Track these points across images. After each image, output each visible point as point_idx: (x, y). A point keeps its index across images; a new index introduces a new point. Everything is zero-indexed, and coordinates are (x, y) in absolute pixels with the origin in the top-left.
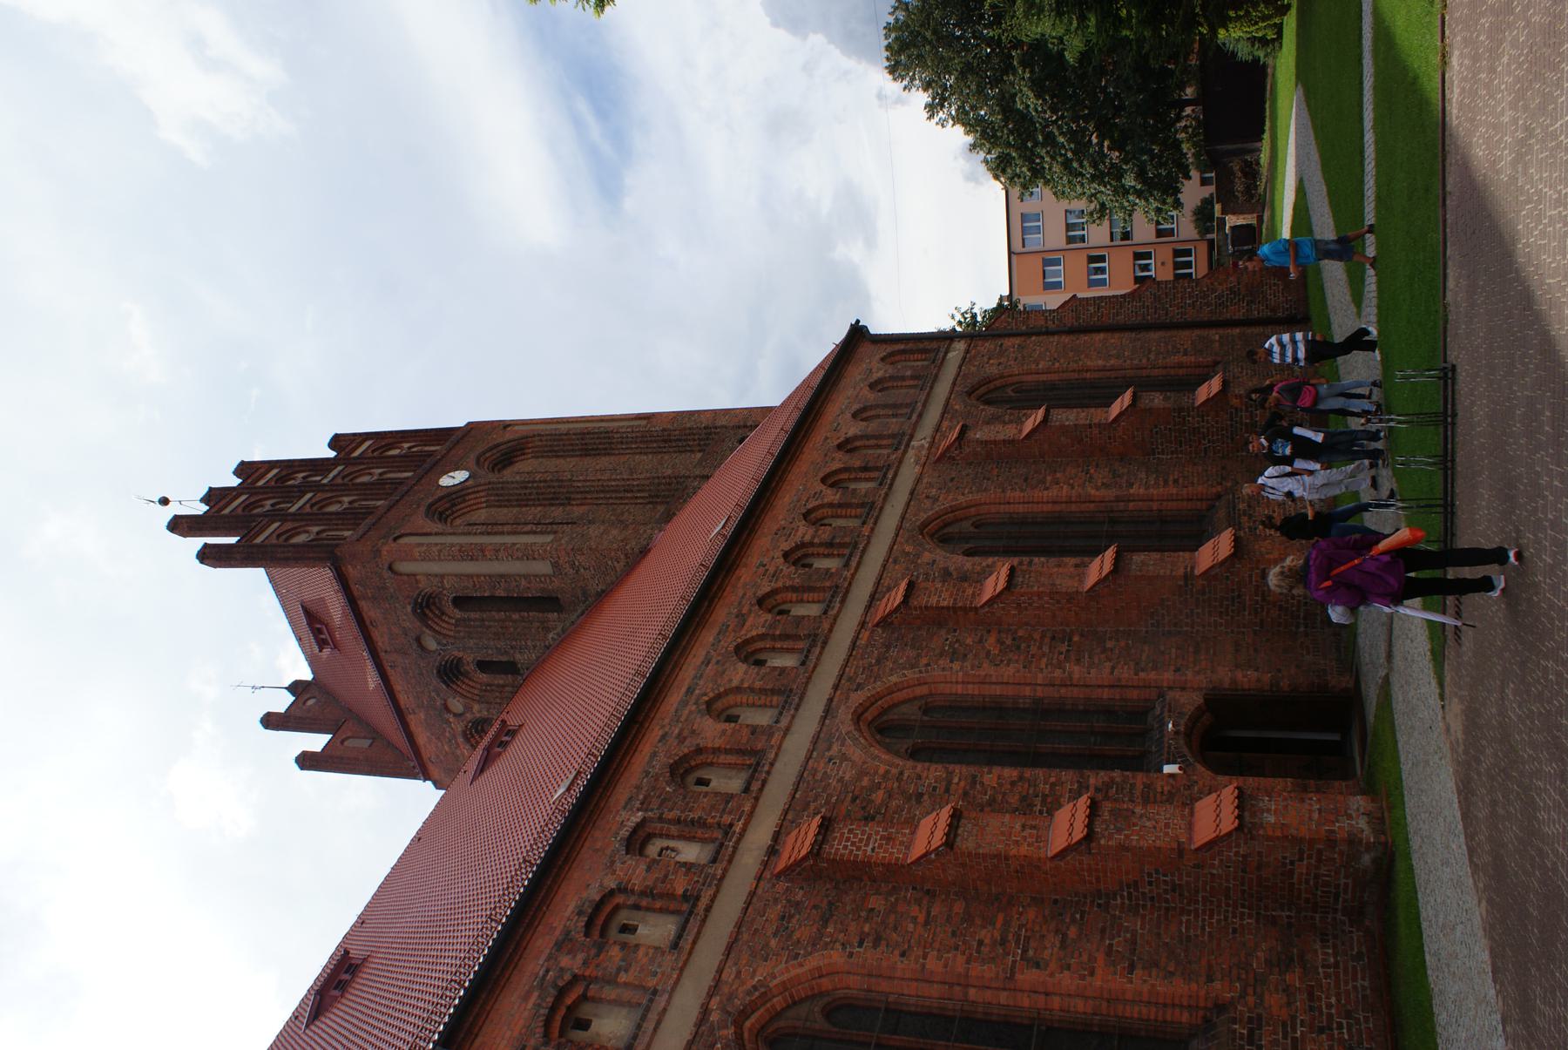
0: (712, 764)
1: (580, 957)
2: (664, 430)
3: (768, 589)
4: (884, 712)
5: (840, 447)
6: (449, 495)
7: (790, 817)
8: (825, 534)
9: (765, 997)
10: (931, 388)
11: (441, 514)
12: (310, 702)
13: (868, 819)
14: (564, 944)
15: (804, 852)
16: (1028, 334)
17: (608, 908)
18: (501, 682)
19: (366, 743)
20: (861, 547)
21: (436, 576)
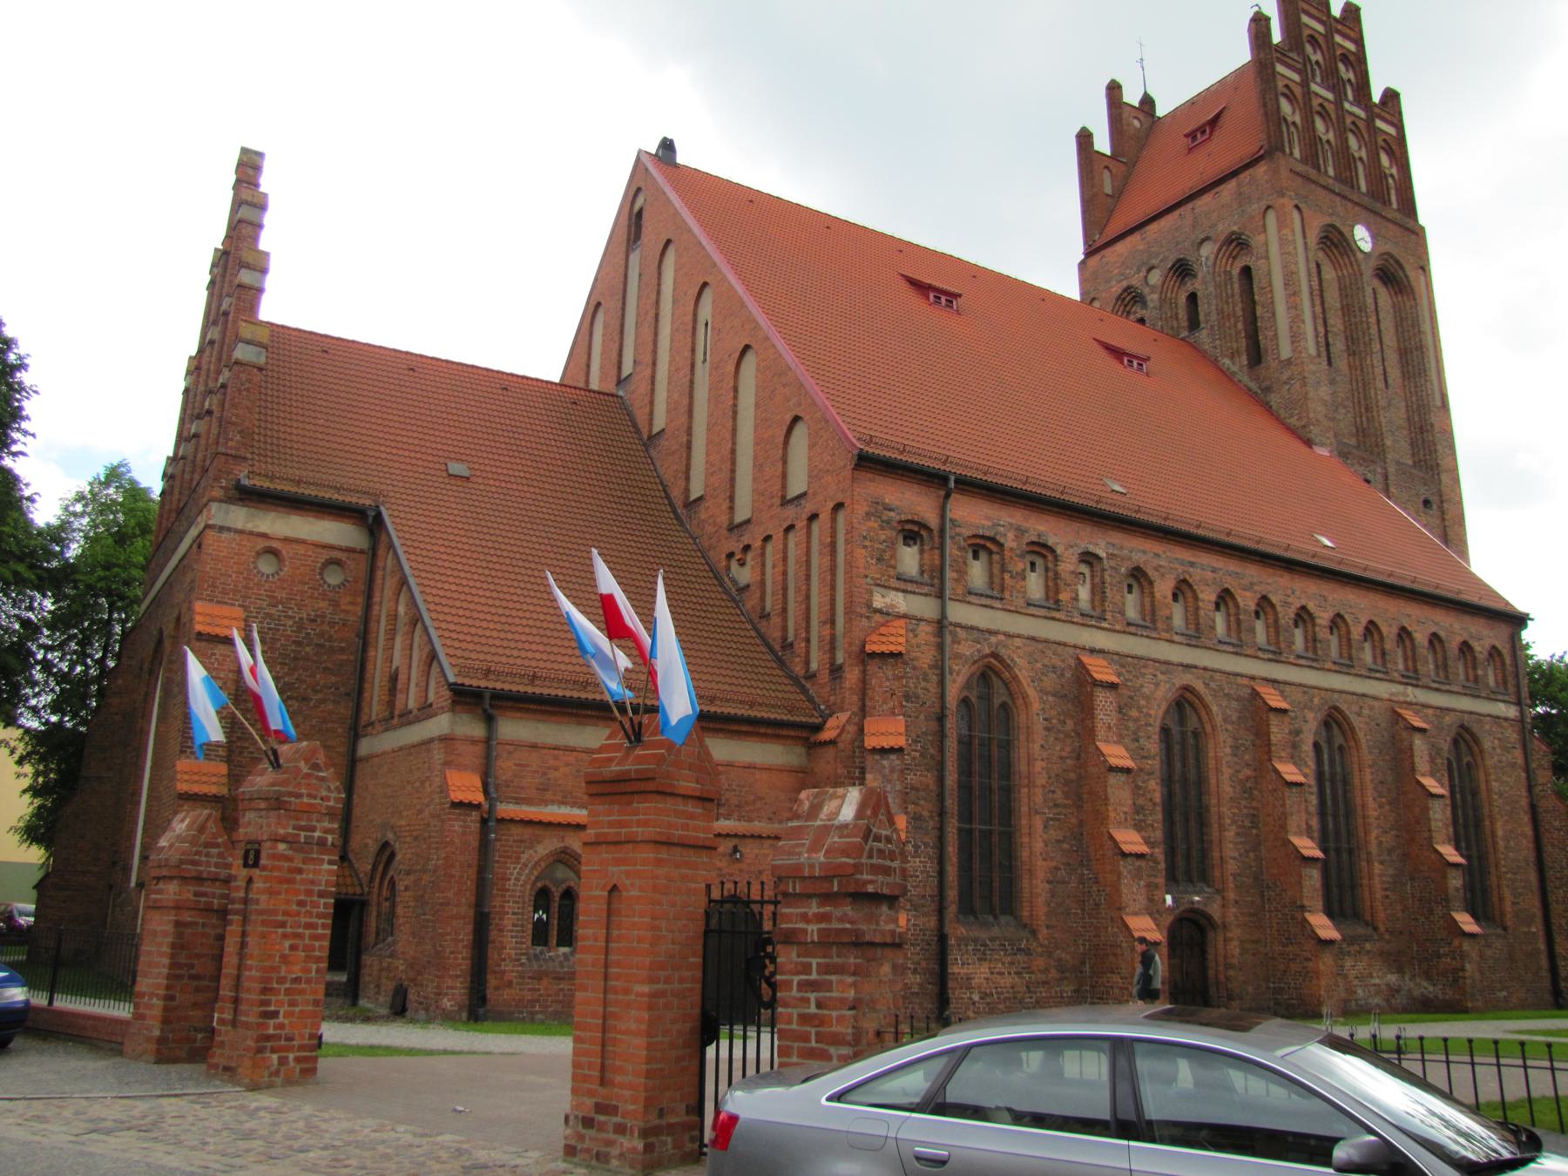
0: (1143, 592)
1: (1014, 545)
2: (1432, 425)
3: (1274, 601)
4: (1192, 705)
5: (1403, 629)
6: (1346, 240)
7: (1115, 657)
8: (1323, 634)
9: (1008, 667)
10: (1465, 694)
11: (1326, 237)
12: (1136, 123)
13: (1120, 710)
14: (1020, 531)
15: (1095, 675)
16: (1527, 769)
17: (1044, 552)
18: (1180, 316)
19: (1108, 190)
20: (1314, 664)
21: (1267, 251)
